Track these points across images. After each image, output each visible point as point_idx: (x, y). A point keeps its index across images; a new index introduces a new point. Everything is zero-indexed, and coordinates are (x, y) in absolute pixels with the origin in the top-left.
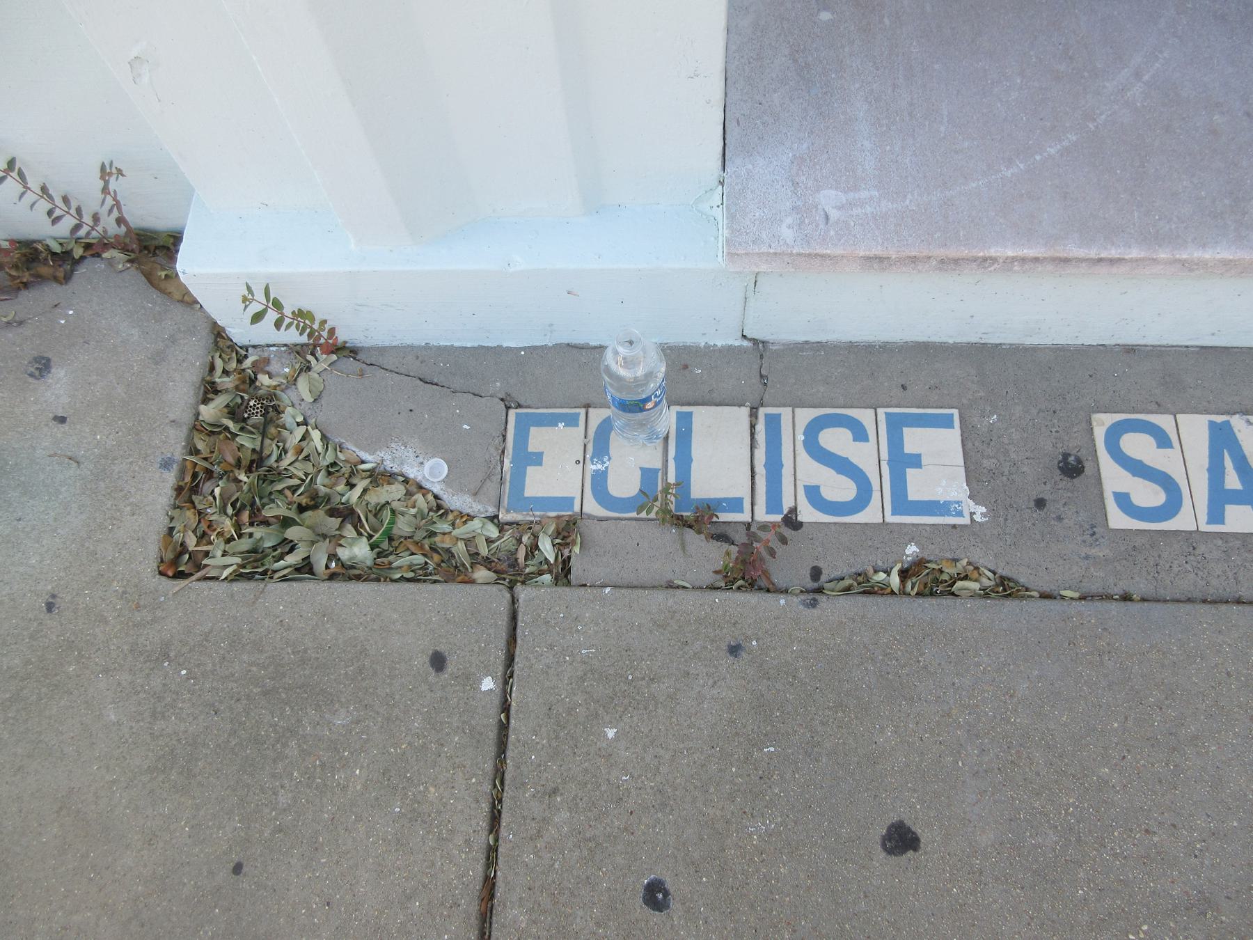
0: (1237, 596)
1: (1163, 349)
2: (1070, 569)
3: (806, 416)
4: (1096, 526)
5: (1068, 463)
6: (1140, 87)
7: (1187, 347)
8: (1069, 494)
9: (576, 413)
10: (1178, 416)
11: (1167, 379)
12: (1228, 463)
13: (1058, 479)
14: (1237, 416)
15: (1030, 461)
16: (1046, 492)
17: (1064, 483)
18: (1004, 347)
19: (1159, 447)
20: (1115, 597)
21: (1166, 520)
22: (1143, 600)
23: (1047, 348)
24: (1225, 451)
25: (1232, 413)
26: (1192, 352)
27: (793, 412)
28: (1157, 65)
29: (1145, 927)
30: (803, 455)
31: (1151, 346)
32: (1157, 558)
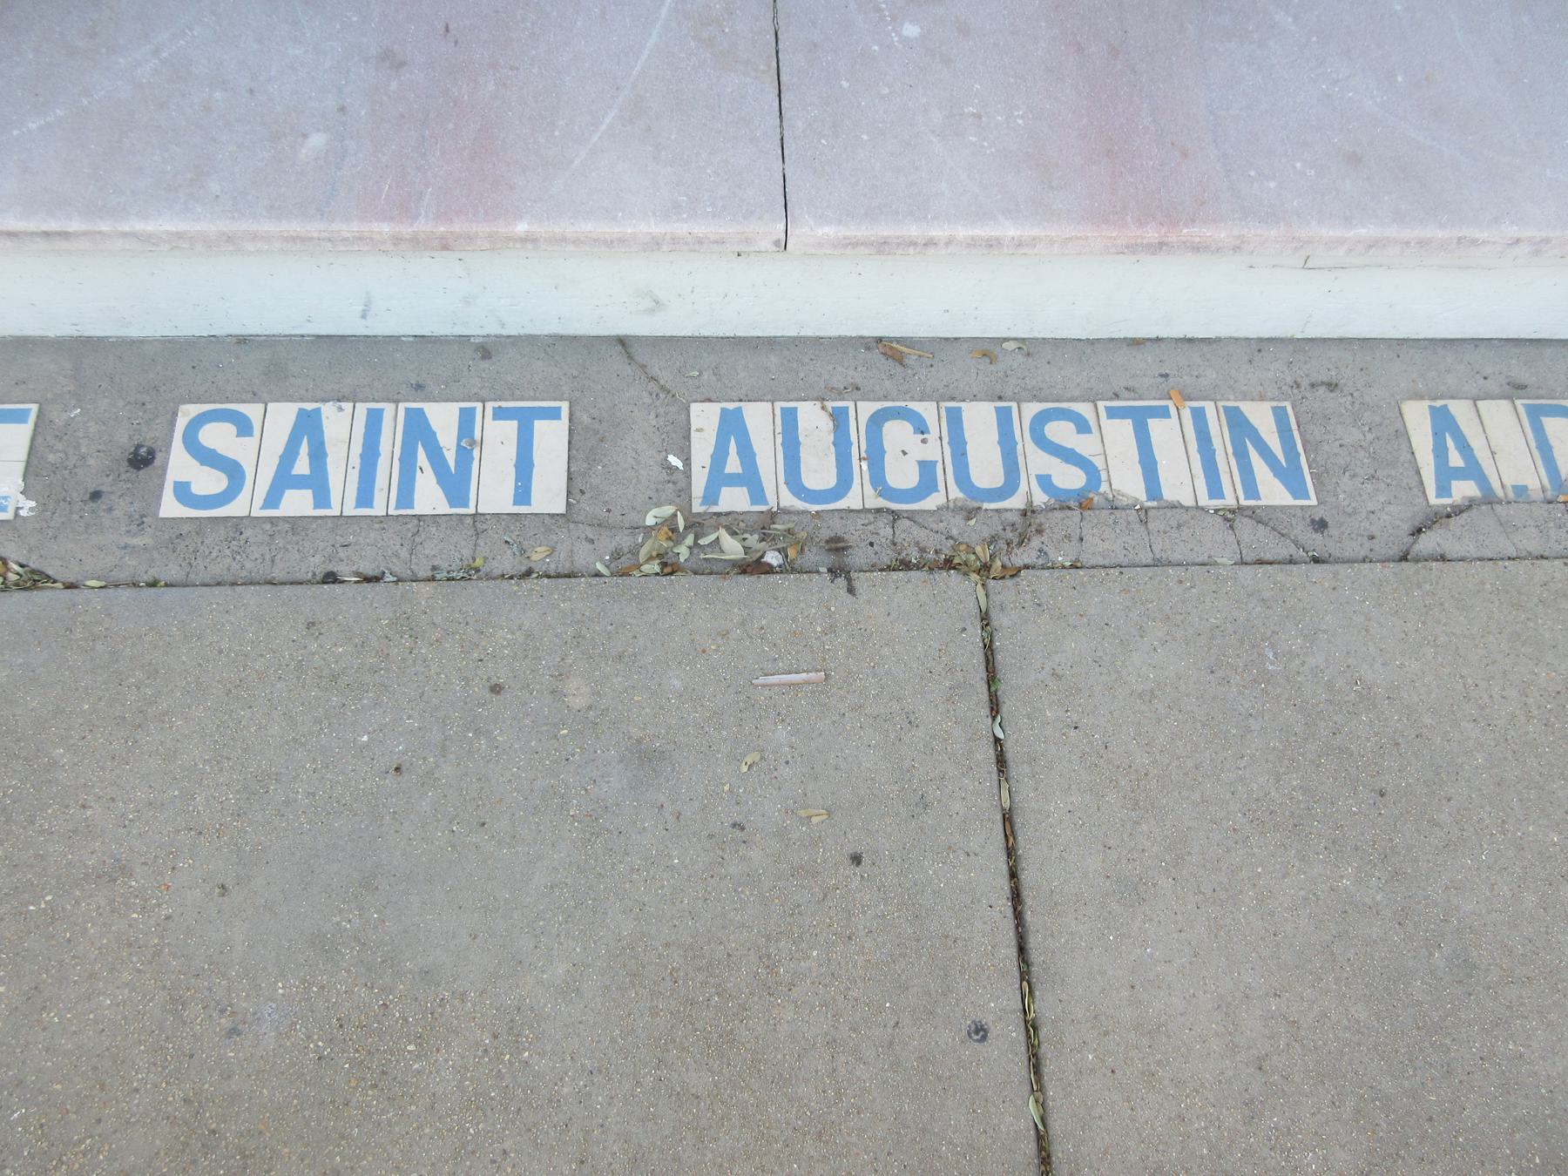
0: (269, 577)
1: (278, 339)
2: (104, 559)
3: (1032, 409)
4: (143, 518)
5: (138, 455)
6: (154, 64)
7: (303, 336)
8: (130, 486)
9: (1225, 412)
10: (858, 403)
11: (272, 368)
12: (304, 449)
13: (122, 470)
14: (331, 403)
15: (101, 454)
16: (105, 485)
17: (129, 474)
18: (472, 340)
19: (1079, 432)
20: (141, 584)
21: (920, 500)
22: (166, 585)
23: (156, 340)
24: (1447, 435)
25: (324, 401)
26: (307, 342)
27: (856, 405)
28: (182, 42)
29: (49, 898)
30: (1030, 446)
31: (496, 336)
32: (200, 545)
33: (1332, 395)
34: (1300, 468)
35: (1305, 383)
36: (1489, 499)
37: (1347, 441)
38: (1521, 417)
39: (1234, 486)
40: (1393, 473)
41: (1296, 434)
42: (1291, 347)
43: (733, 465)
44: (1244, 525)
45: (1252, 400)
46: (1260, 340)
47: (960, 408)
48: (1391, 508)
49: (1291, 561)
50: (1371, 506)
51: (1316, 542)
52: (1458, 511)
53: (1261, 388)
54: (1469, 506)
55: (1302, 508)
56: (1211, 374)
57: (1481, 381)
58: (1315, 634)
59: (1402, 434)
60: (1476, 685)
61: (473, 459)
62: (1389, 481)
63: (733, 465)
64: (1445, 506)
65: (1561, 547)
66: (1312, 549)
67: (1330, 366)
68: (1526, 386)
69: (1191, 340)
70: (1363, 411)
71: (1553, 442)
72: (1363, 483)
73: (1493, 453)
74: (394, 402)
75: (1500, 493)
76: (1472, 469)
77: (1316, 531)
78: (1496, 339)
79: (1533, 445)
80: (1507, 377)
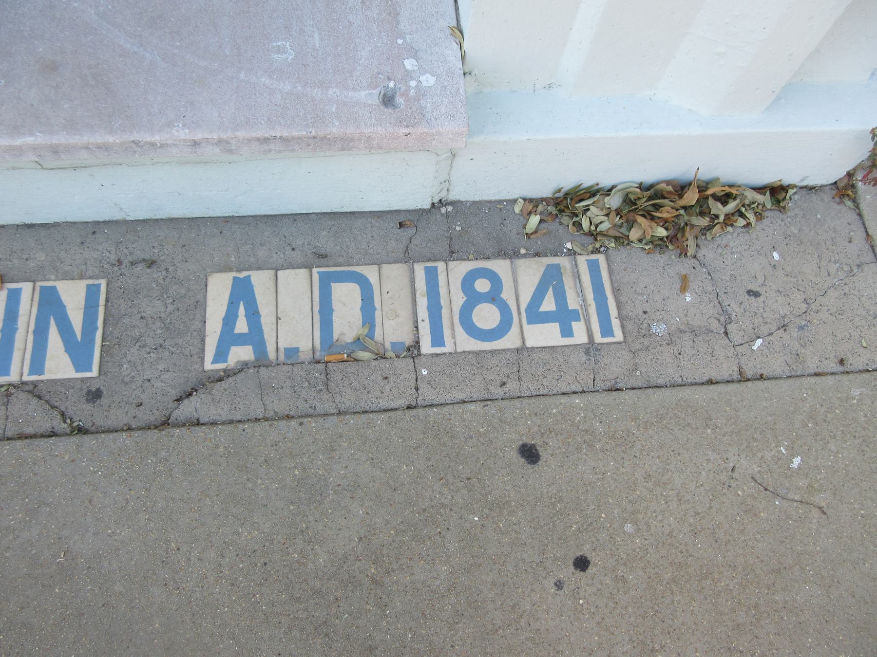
12: (242, 311)
33: (148, 271)
34: (92, 342)
35: (126, 261)
36: (261, 362)
37: (149, 312)
38: (313, 285)
39: (23, 366)
40: (180, 341)
41: (101, 310)
42: (124, 228)
43: (242, 326)
44: (20, 399)
45: (72, 279)
46: (98, 223)
47: (436, 267)
48: (166, 376)
49: (53, 434)
50: (148, 375)
51: (82, 412)
52: (228, 373)
53: (83, 267)
54: (244, 366)
55: (82, 380)
56: (41, 256)
57: (290, 251)
58: (38, 507)
59: (200, 305)
60: (178, 549)
61: (375, 309)
62: (174, 350)
63: (242, 326)
64: (218, 371)
65: (307, 406)
66: (78, 419)
67: (155, 244)
68: (326, 256)
69: (31, 226)
70: (173, 284)
71: (336, 305)
72: (149, 353)
73: (278, 318)
74: (33, 281)
75: (272, 355)
76: (255, 337)
77: (88, 401)
78: (313, 213)
79: (317, 308)
80: (315, 247)
